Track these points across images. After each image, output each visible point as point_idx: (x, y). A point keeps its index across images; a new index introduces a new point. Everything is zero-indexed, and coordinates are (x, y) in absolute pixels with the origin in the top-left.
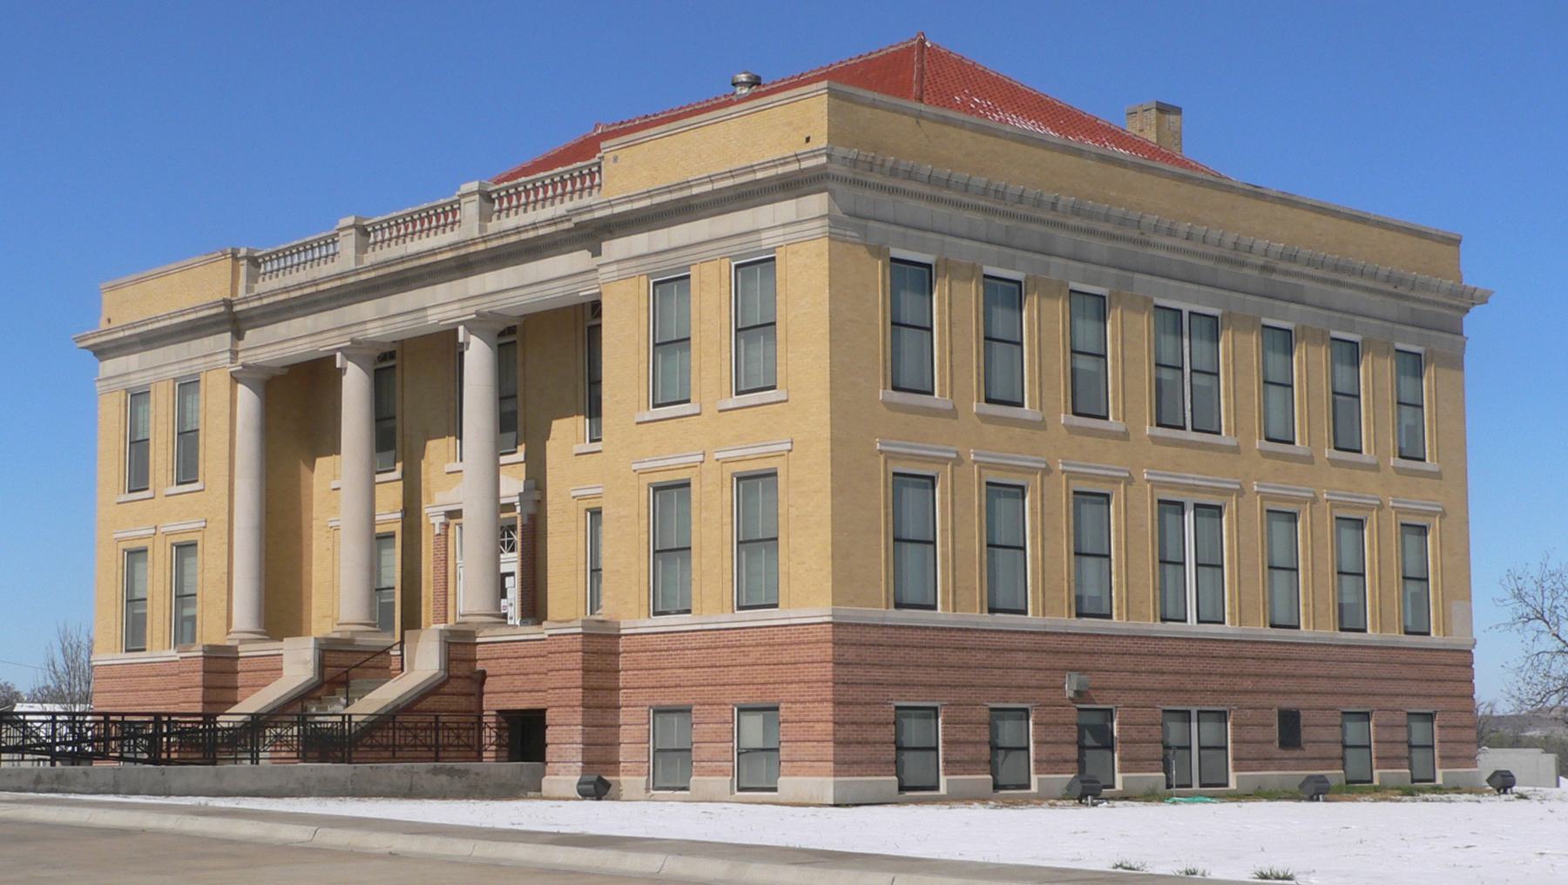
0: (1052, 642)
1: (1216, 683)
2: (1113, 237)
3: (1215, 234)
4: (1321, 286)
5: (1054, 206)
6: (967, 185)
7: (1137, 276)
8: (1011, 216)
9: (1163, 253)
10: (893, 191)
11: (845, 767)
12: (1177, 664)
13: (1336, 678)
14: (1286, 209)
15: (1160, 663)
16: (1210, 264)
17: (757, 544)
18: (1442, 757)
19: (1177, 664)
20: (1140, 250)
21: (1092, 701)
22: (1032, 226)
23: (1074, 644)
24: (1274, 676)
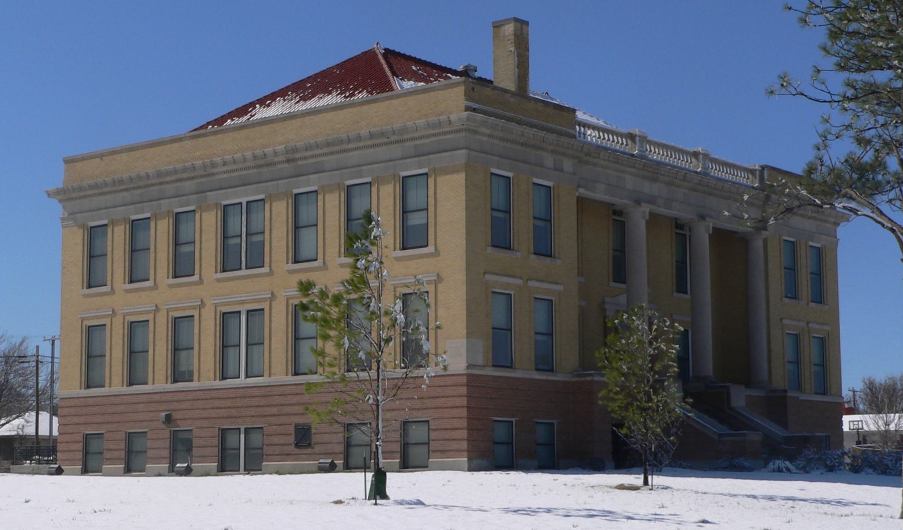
0: (157, 397)
1: (252, 412)
2: (193, 178)
4: (334, 157)
6: (148, 176)
7: (208, 194)
8: (140, 187)
10: (85, 197)
12: (229, 403)
14: (312, 117)
15: (217, 403)
19: (229, 403)
22: (152, 188)
23: (169, 397)
24: (294, 404)
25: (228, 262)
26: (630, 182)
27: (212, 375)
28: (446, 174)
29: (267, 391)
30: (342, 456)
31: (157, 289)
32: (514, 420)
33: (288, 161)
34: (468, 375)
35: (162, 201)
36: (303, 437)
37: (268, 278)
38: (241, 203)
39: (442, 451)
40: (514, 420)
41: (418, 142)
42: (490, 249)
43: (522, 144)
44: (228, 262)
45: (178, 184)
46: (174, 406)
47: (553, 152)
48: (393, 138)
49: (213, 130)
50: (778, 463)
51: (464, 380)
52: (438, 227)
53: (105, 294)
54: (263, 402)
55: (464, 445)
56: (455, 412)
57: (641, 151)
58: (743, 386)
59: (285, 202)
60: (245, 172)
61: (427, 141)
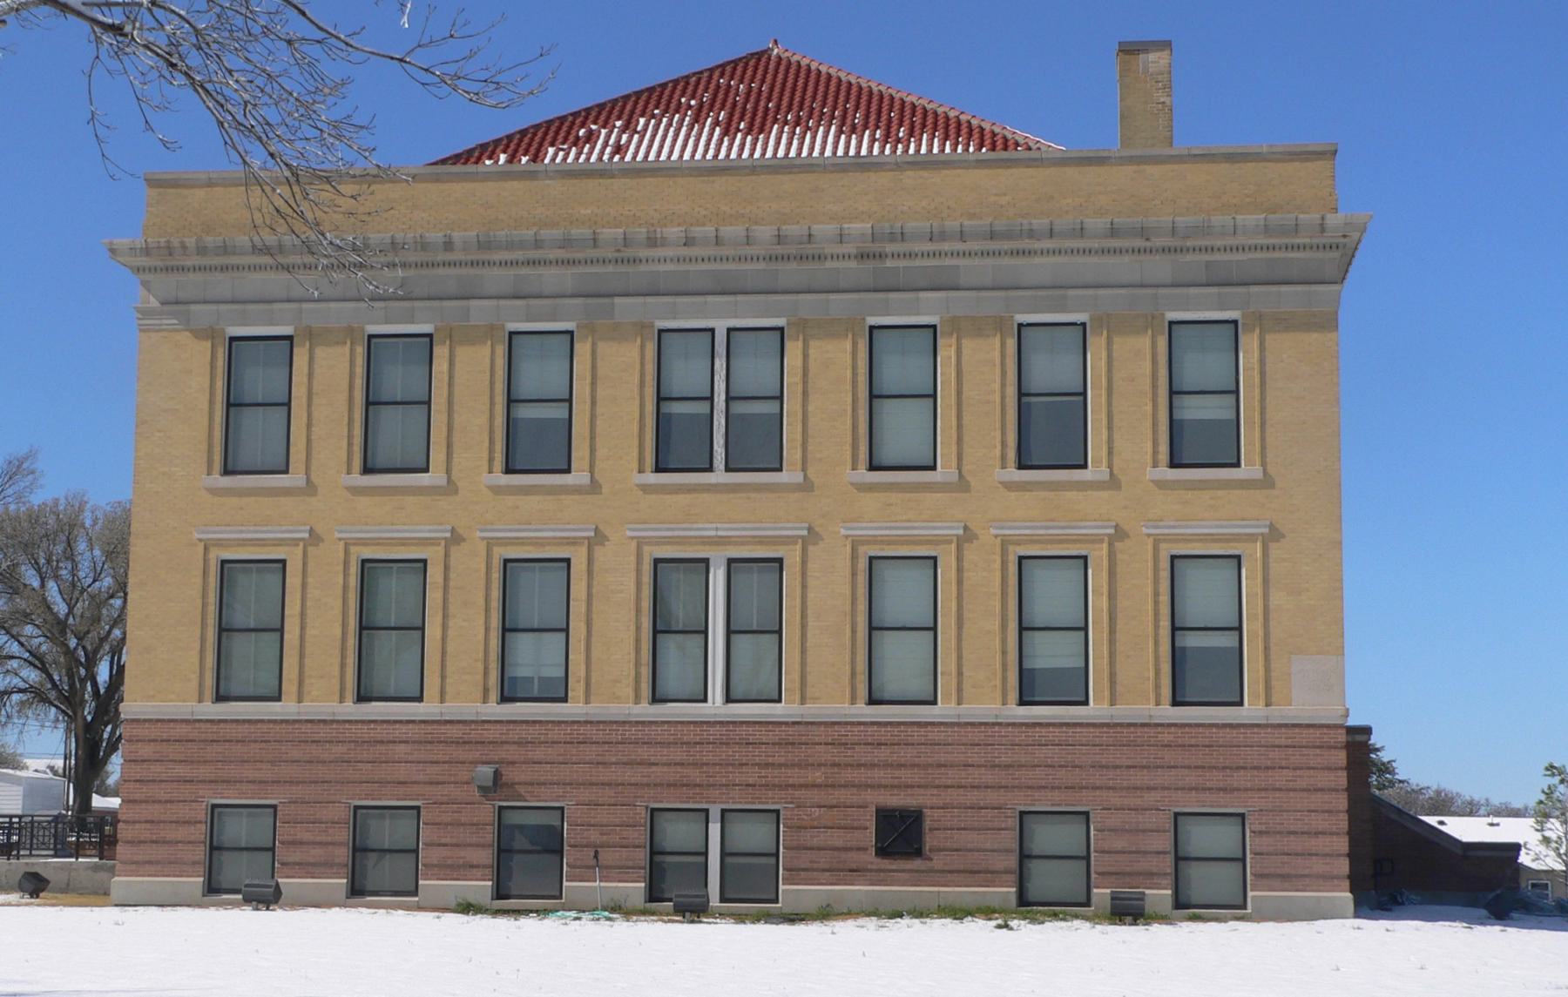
3: (732, 231)
5: (448, 245)
7: (617, 300)
9: (670, 267)
11: (133, 867)
13: (1008, 766)
14: (925, 174)
16: (762, 266)
17: (758, 626)
18: (1257, 876)
19: (678, 754)
20: (630, 269)
21: (520, 798)
23: (492, 733)
25: (673, 446)
27: (630, 692)
28: (1287, 329)
29: (796, 734)
31: (456, 492)
33: (862, 256)
35: (473, 303)
36: (900, 835)
37: (1105, 494)
38: (712, 331)
39: (1285, 877)
41: (1217, 257)
44: (673, 446)
45: (524, 271)
46: (510, 752)
48: (1158, 242)
49: (979, 156)
52: (1269, 430)
53: (577, 490)
54: (780, 756)
55: (1344, 866)
56: (1318, 800)
59: (848, 345)
60: (732, 266)
61: (1240, 256)
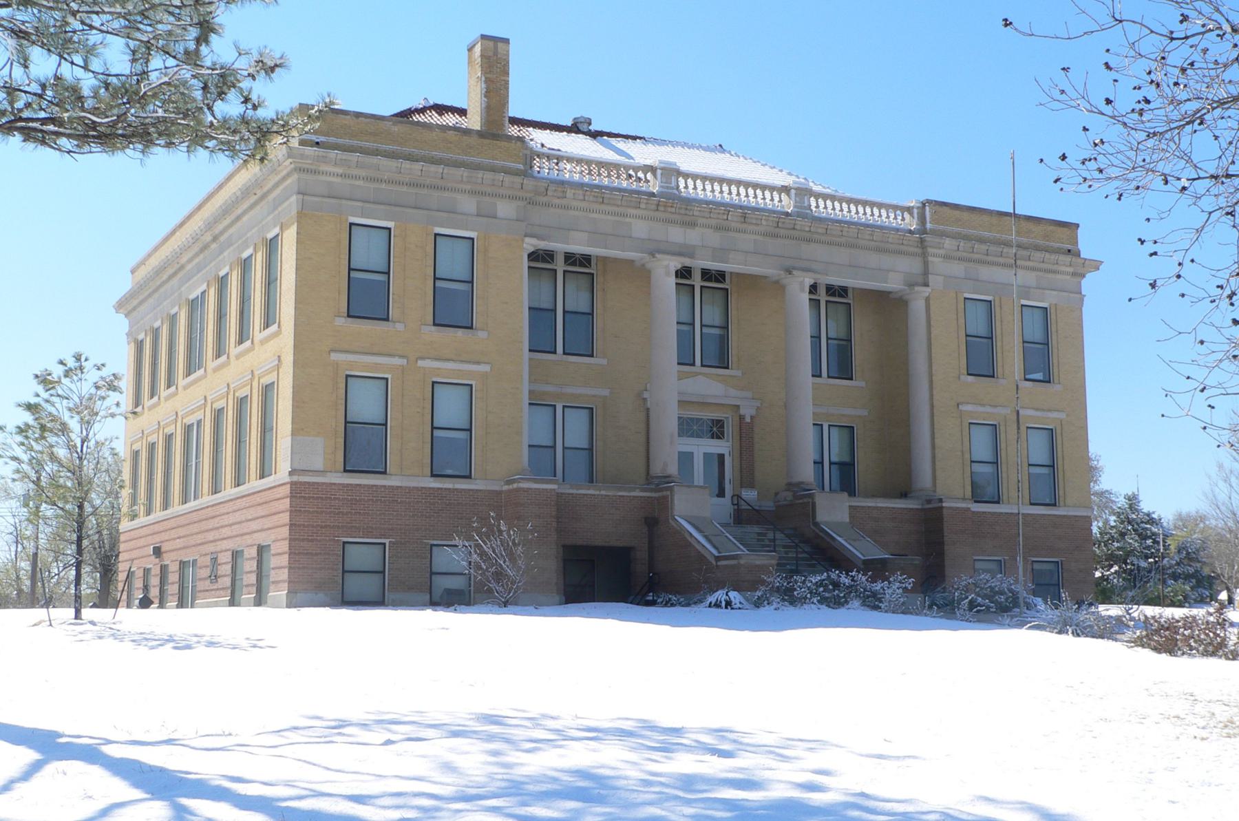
26: (640, 229)
30: (255, 589)
32: (387, 541)
34: (292, 483)
40: (387, 541)
42: (341, 321)
43: (409, 185)
46: (157, 539)
47: (473, 193)
50: (720, 595)
51: (286, 490)
57: (801, 207)
58: (846, 494)
